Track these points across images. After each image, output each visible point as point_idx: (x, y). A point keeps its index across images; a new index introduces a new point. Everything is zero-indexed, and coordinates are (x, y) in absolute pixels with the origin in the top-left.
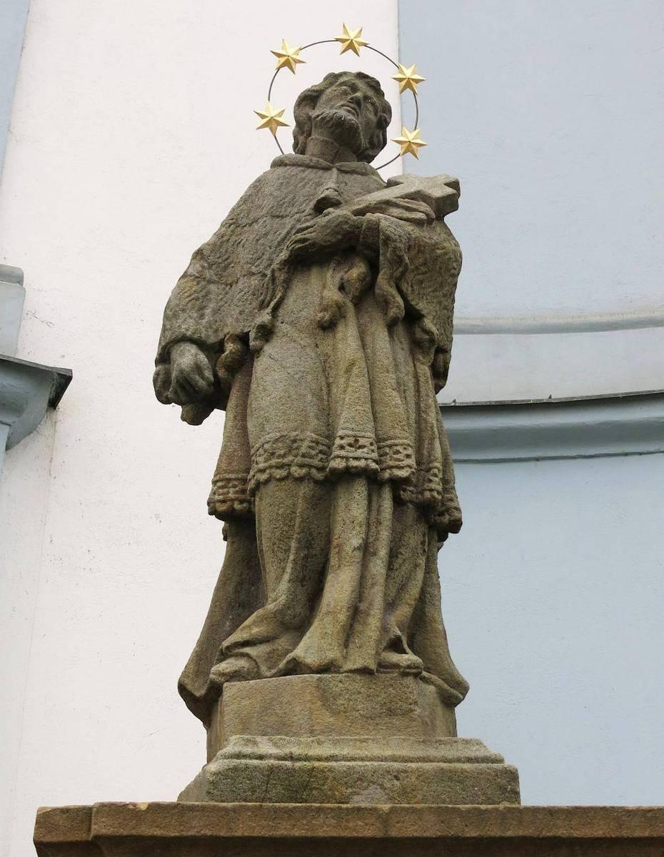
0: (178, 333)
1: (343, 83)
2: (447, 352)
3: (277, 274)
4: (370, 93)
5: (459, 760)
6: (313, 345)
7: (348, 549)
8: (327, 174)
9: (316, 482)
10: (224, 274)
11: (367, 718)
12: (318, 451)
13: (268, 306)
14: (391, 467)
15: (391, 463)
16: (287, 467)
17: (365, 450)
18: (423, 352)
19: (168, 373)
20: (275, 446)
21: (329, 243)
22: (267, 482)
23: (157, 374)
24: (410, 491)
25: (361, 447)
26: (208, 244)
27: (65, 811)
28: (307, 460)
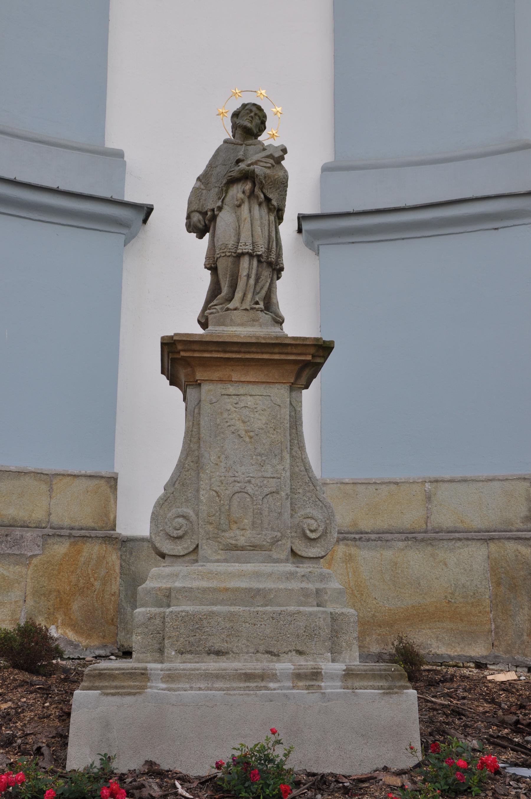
0: (193, 209)
4: (257, 112)
7: (243, 276)
9: (234, 257)
19: (190, 222)
22: (219, 257)
26: (201, 175)
27: (167, 336)
28: (231, 250)
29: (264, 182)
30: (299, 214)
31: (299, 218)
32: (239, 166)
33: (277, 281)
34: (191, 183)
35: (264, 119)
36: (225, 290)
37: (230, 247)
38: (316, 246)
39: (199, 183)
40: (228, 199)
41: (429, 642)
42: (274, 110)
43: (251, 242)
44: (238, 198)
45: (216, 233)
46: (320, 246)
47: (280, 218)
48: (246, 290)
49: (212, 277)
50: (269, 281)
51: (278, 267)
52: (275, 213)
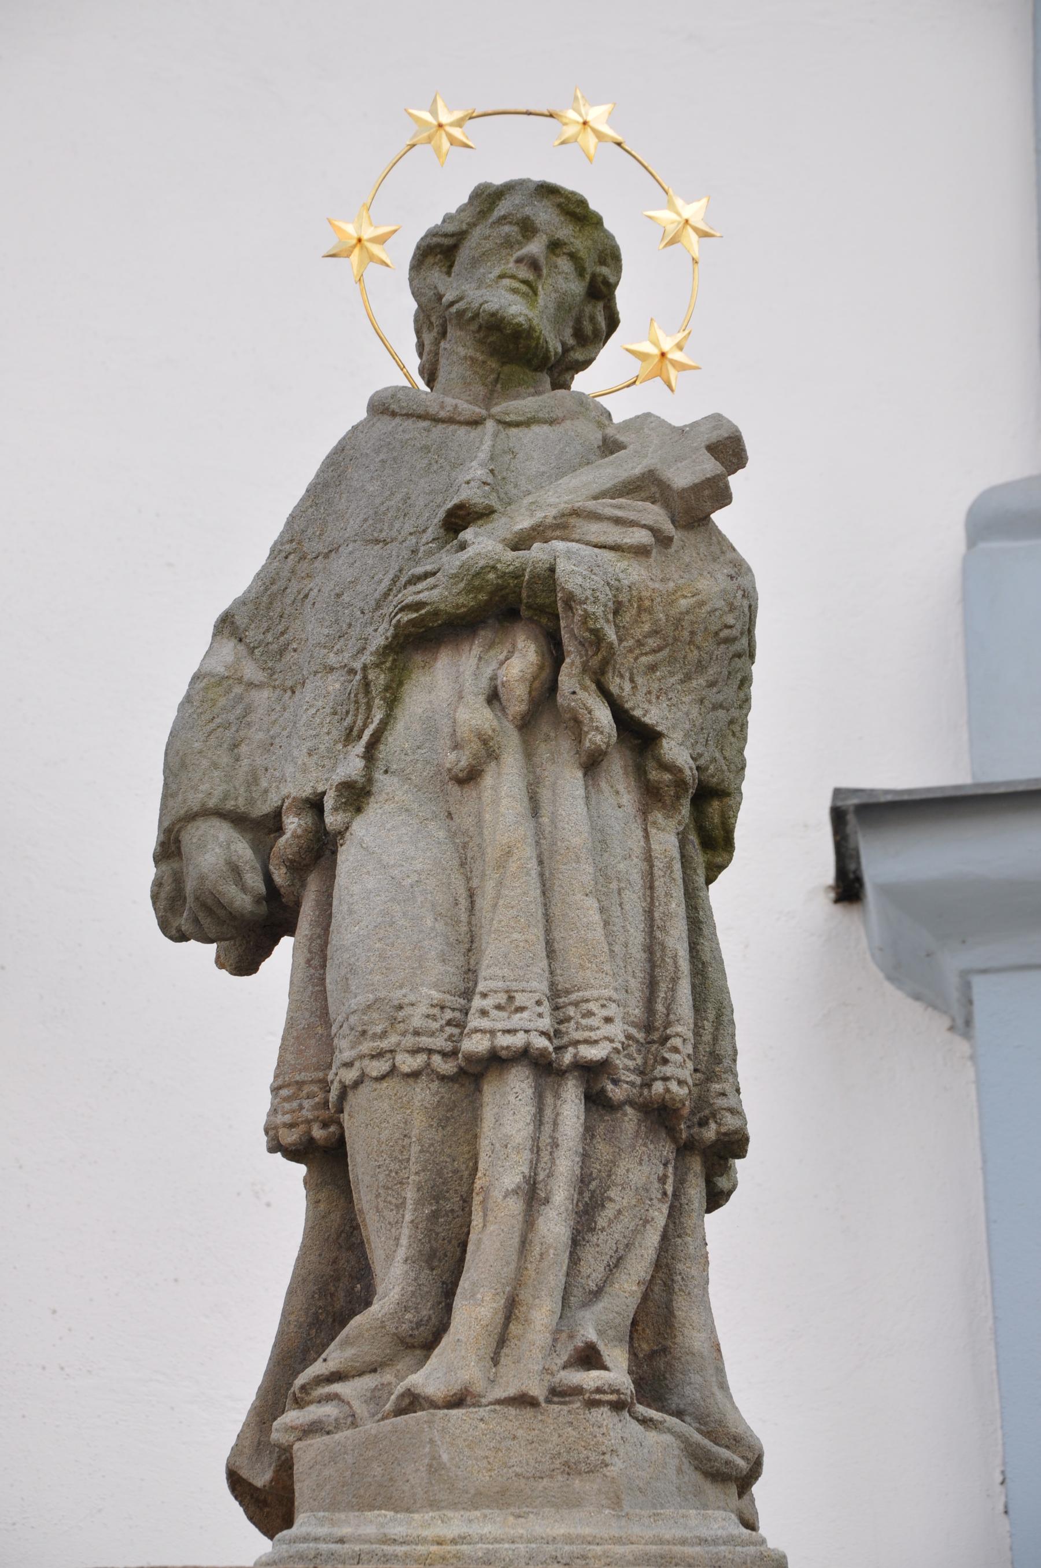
0: (194, 800)
1: (504, 217)
2: (728, 795)
3: (371, 676)
4: (565, 232)
5: (683, 1542)
6: (443, 815)
7: (497, 1194)
8: (474, 433)
9: (443, 1078)
10: (279, 666)
11: (528, 1478)
12: (444, 1022)
13: (360, 737)
14: (576, 1043)
15: (578, 1035)
16: (388, 1055)
17: (525, 1014)
18: (664, 806)
19: (178, 879)
20: (366, 1018)
21: (463, 610)
22: (357, 1084)
23: (158, 884)
24: (627, 1082)
25: (521, 1009)
26: (241, 602)
28: (425, 1041)
29: (611, 635)
30: (838, 793)
31: (838, 816)
32: (463, 546)
33: (712, 1221)
34: (185, 647)
35: (604, 270)
36: (395, 1277)
37: (417, 1022)
38: (953, 981)
39: (229, 649)
40: (399, 740)
41: (449, 1128)
42: (665, 215)
43: (544, 987)
44: (463, 732)
45: (334, 939)
46: (979, 983)
47: (712, 842)
48: (518, 1281)
49: (313, 1203)
50: (660, 1216)
51: (710, 1133)
52: (685, 809)
